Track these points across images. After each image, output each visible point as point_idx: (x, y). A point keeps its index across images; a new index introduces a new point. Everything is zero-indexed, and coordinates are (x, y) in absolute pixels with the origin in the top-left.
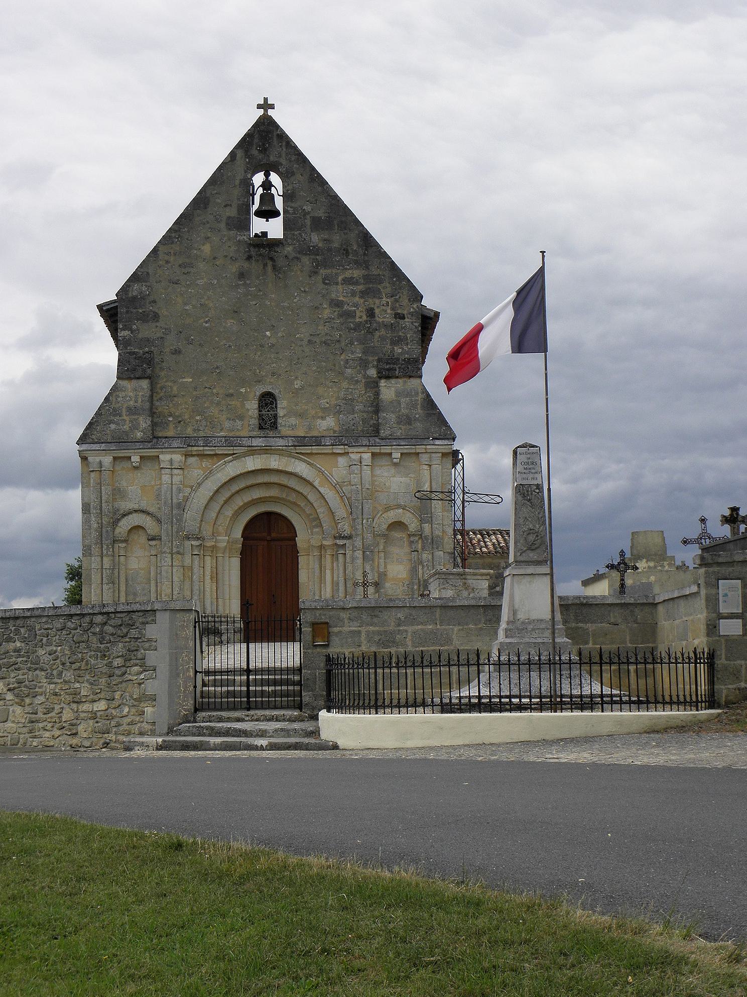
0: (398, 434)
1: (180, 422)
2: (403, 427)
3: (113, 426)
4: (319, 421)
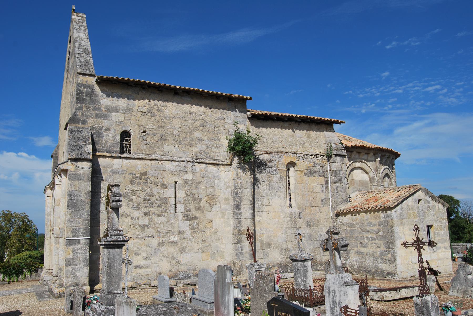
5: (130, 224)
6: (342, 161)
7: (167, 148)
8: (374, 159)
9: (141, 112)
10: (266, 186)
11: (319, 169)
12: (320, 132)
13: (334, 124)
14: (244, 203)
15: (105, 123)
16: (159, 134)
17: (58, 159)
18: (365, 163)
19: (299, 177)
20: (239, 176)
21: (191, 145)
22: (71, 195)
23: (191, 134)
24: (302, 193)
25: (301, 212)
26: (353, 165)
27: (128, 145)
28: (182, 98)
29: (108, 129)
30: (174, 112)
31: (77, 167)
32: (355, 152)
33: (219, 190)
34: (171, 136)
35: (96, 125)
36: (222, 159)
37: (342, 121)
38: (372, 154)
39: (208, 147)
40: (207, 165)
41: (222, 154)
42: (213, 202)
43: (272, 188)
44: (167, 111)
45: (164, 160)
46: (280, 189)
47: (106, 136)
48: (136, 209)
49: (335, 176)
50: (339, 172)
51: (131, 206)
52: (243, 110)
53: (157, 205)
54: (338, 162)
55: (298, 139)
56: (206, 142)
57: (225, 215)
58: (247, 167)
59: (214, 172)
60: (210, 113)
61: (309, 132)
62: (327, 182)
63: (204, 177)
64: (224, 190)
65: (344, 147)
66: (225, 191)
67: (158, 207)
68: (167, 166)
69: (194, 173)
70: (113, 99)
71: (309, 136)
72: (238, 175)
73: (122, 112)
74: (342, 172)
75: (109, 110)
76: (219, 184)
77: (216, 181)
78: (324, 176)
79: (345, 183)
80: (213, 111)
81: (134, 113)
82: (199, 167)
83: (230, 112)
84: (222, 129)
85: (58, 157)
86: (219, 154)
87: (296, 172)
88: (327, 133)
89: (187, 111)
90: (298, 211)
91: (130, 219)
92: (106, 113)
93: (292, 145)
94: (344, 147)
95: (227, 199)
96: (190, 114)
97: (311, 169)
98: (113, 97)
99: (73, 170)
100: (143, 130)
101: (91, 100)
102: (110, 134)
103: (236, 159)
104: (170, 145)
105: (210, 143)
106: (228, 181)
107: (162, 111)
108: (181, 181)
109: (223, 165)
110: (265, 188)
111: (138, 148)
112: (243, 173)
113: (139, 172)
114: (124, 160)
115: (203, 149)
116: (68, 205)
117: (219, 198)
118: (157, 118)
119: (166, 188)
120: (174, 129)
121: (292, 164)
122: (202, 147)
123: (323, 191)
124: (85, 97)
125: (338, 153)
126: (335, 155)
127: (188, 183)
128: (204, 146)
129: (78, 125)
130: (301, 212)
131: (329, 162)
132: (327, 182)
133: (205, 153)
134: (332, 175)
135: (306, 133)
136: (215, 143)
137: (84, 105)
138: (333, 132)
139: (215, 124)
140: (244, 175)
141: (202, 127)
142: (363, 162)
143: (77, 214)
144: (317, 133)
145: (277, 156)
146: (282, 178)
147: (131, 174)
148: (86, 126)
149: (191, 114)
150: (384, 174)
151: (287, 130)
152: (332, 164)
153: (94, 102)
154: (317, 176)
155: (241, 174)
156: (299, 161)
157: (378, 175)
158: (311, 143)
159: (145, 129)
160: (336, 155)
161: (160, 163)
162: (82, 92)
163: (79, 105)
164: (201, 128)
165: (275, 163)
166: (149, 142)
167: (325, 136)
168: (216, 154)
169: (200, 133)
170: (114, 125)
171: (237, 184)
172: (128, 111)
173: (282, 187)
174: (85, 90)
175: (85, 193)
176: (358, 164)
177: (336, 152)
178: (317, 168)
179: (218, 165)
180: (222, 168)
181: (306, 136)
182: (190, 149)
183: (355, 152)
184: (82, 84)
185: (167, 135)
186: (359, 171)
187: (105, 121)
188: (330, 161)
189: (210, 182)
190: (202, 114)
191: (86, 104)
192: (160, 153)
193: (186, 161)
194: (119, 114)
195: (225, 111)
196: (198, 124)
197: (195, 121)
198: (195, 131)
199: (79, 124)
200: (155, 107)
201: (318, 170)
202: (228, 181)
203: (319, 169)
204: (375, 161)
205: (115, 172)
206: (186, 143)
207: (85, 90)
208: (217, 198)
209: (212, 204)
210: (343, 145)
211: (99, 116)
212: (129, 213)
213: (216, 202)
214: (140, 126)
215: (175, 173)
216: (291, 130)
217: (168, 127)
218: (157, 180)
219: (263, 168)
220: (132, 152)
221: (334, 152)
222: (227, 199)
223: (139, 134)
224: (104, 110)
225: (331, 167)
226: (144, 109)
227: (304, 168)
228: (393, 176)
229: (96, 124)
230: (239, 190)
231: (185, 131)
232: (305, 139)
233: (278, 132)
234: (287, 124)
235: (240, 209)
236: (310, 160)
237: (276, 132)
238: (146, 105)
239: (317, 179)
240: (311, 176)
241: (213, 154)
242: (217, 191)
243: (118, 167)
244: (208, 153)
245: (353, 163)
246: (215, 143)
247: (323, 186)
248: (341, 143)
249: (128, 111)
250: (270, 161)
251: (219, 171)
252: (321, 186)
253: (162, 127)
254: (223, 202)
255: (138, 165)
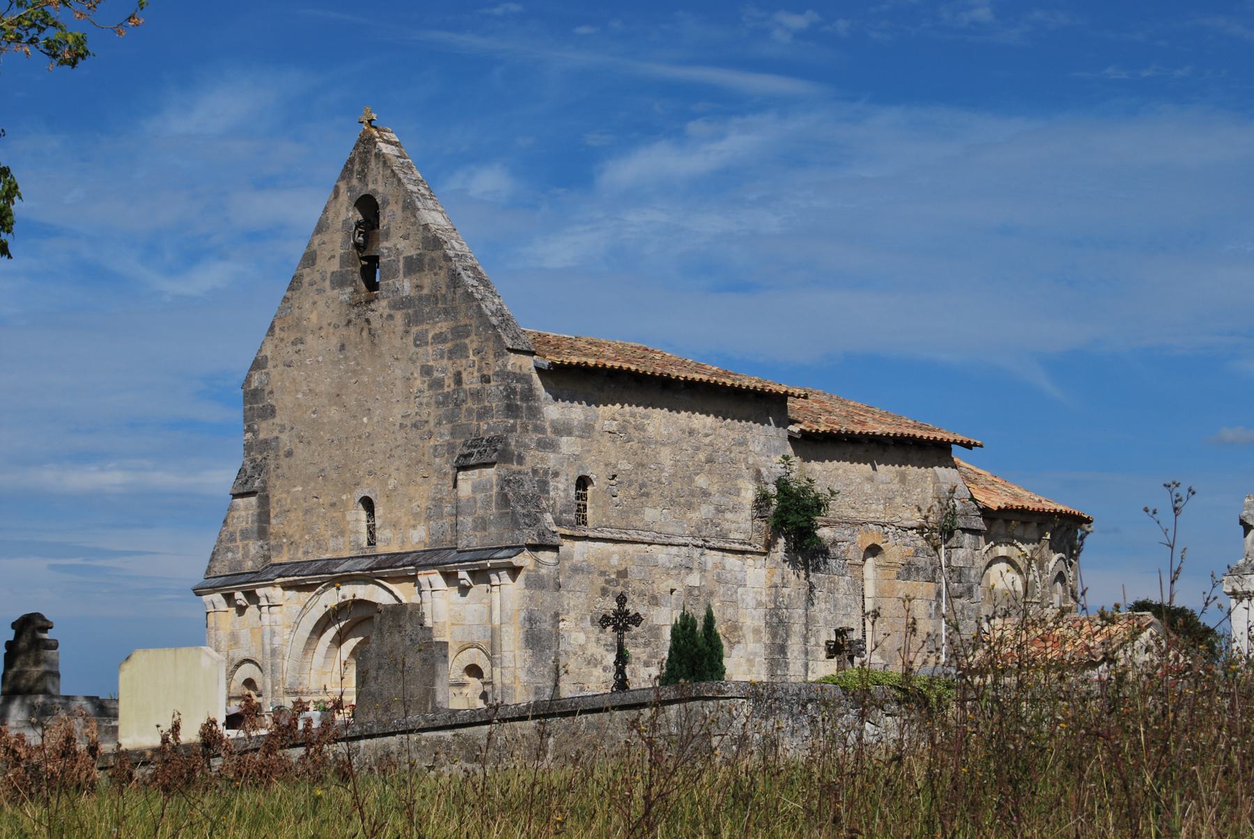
0: (474, 544)
1: (291, 544)
2: (478, 534)
3: (230, 555)
4: (412, 532)
5: (601, 680)
6: (975, 544)
7: (650, 514)
8: (1036, 537)
9: (610, 432)
10: (826, 602)
11: (926, 562)
12: (926, 468)
13: (953, 446)
14: (793, 641)
15: (552, 460)
16: (636, 481)
17: (268, 504)
18: (1017, 547)
19: (885, 581)
20: (785, 581)
21: (690, 506)
22: (531, 619)
23: (691, 480)
24: (891, 620)
25: (887, 665)
26: (992, 552)
27: (582, 507)
28: (676, 396)
29: (556, 474)
30: (662, 430)
31: (537, 560)
32: (1001, 521)
33: (745, 611)
34: (657, 485)
35: (539, 466)
36: (742, 536)
37: (978, 442)
38: (1035, 524)
39: (719, 510)
40: (725, 554)
41: (743, 526)
42: (734, 635)
43: (835, 606)
44: (650, 429)
45: (655, 544)
46: (849, 609)
47: (554, 489)
48: (610, 648)
49: (960, 582)
50: (967, 572)
51: (603, 643)
52: (784, 420)
53: (643, 641)
54: (967, 546)
55: (881, 487)
56: (716, 498)
57: (753, 666)
58: (800, 559)
59: (737, 569)
60: (723, 430)
61: (903, 467)
62: (939, 594)
63: (719, 581)
64: (752, 610)
65: (979, 509)
66: (754, 612)
67: (646, 645)
68: (660, 556)
69: (703, 570)
70: (563, 404)
71: (903, 479)
72: (783, 578)
73: (577, 433)
74: (973, 573)
75: (563, 429)
76: (744, 597)
77: (740, 590)
78: (933, 580)
79: (978, 597)
80: (729, 424)
81: (596, 435)
82: (713, 557)
83: (758, 424)
84: (744, 467)
85: (267, 496)
86: (737, 526)
87: (878, 570)
88: (940, 471)
89: (684, 426)
90: (882, 661)
91: (601, 670)
92: (553, 436)
93: (870, 502)
94: (979, 509)
95: (757, 631)
96: (690, 433)
97: (909, 563)
98: (563, 401)
99: (531, 568)
100: (612, 474)
101: (530, 408)
102: (559, 485)
103: (782, 541)
104: (655, 507)
105: (724, 500)
106: (759, 590)
107: (640, 428)
108: (682, 590)
109: (751, 553)
110: (823, 606)
111: (605, 515)
112: (794, 573)
113: (615, 570)
114: (591, 544)
115: (710, 516)
116: (527, 640)
117: (744, 628)
118: (634, 444)
119: (657, 604)
120: (662, 470)
121: (874, 550)
122: (709, 511)
123: (930, 616)
124: (519, 403)
125: (969, 526)
126: (962, 529)
127: (692, 595)
128: (712, 508)
129: (510, 466)
130: (887, 665)
131: (947, 546)
132: (939, 594)
133: (714, 524)
134: (951, 578)
135: (897, 472)
136: (729, 501)
137: (519, 421)
138: (953, 468)
139: (732, 455)
140: (794, 578)
141: (710, 464)
142: (1014, 545)
143: (541, 658)
144: (920, 470)
145: (846, 532)
146: (853, 584)
147: (603, 573)
148: (524, 467)
149: (691, 432)
150: (1055, 574)
151: (862, 464)
152: (953, 550)
153: (534, 412)
154: (921, 579)
155: (790, 576)
156: (887, 542)
157: (1044, 577)
158: (907, 495)
159: (615, 472)
160: (964, 530)
161: (649, 548)
162: (514, 391)
163: (512, 421)
164: (707, 467)
165: (843, 548)
166: (621, 500)
167: (936, 479)
168: (734, 526)
169: (705, 478)
170: (565, 465)
171: (783, 597)
172: (587, 429)
173: (853, 605)
174: (519, 387)
175: (551, 616)
176: (1002, 550)
177: (965, 524)
178: (922, 561)
179: (743, 552)
180: (750, 560)
181: (898, 479)
182: (689, 515)
183: (1001, 521)
184: (514, 373)
185: (651, 485)
186: (1003, 566)
187: (551, 455)
188: (949, 543)
189: (729, 593)
190: (710, 432)
191: (522, 417)
192: (638, 524)
193: (691, 546)
194: (573, 438)
195: (751, 423)
196: (702, 456)
197: (698, 449)
198: (698, 474)
199: (513, 464)
200: (632, 420)
201: (922, 564)
202: (759, 590)
203: (926, 562)
204: (1039, 542)
205: (576, 570)
206: (682, 500)
207: (519, 387)
208: (741, 628)
209: (733, 640)
210: (976, 504)
211: (544, 445)
212: (599, 657)
213: (739, 636)
214: (606, 465)
215: (673, 572)
216: (869, 464)
217: (652, 466)
218: (643, 587)
219: (821, 559)
220: (590, 525)
221: (961, 522)
222: (757, 631)
223: (606, 483)
224: (549, 430)
225: (949, 559)
226: (614, 426)
227: (897, 560)
228: (1071, 579)
229: (538, 463)
230: (784, 610)
231: (680, 474)
232: (896, 486)
233: (845, 471)
234: (860, 451)
235: (785, 654)
236: (908, 540)
237: (840, 471)
238: (617, 416)
239: (921, 588)
240: (908, 579)
241: (726, 526)
242: (740, 611)
243: (582, 559)
244: (719, 524)
245: (992, 546)
246: (729, 501)
247: (931, 605)
248: (972, 498)
249: (587, 429)
250: (834, 543)
251: (746, 567)
252: (928, 603)
253: (643, 465)
254: (750, 637)
255: (613, 553)
